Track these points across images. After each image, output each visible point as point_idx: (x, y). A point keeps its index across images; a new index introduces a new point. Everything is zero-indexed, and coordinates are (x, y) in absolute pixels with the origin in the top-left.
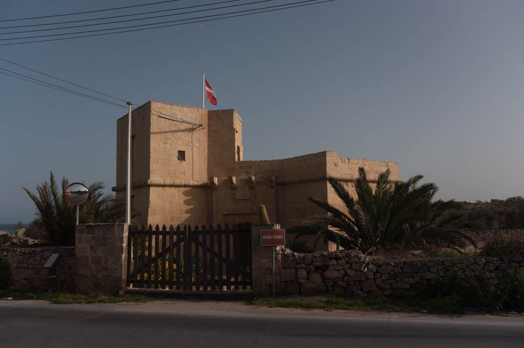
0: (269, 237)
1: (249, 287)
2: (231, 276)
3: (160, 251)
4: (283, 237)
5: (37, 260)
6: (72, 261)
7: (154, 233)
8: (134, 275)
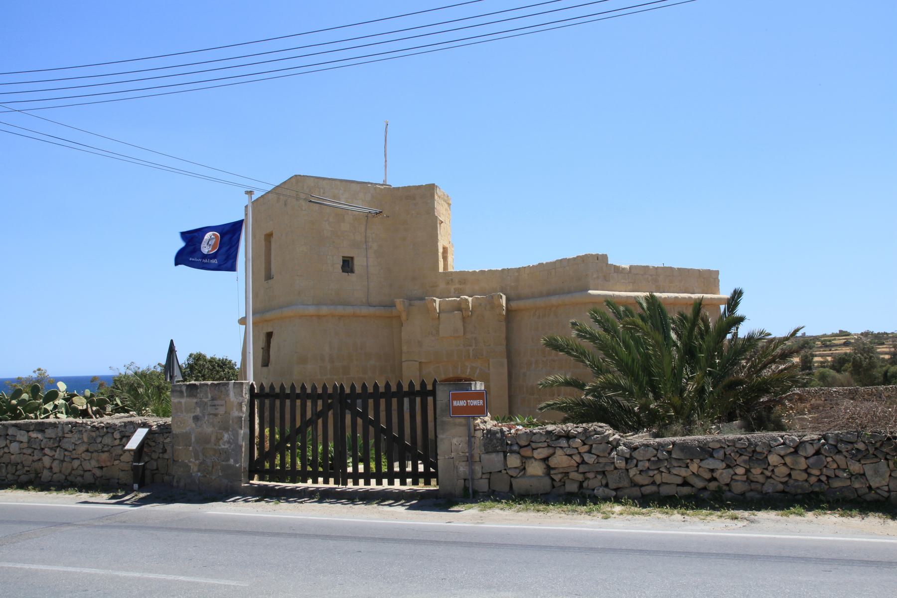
0: (462, 403)
1: (433, 481)
2: (359, 463)
3: (298, 424)
4: (484, 403)
5: (116, 439)
6: (168, 440)
7: (298, 396)
8: (261, 461)
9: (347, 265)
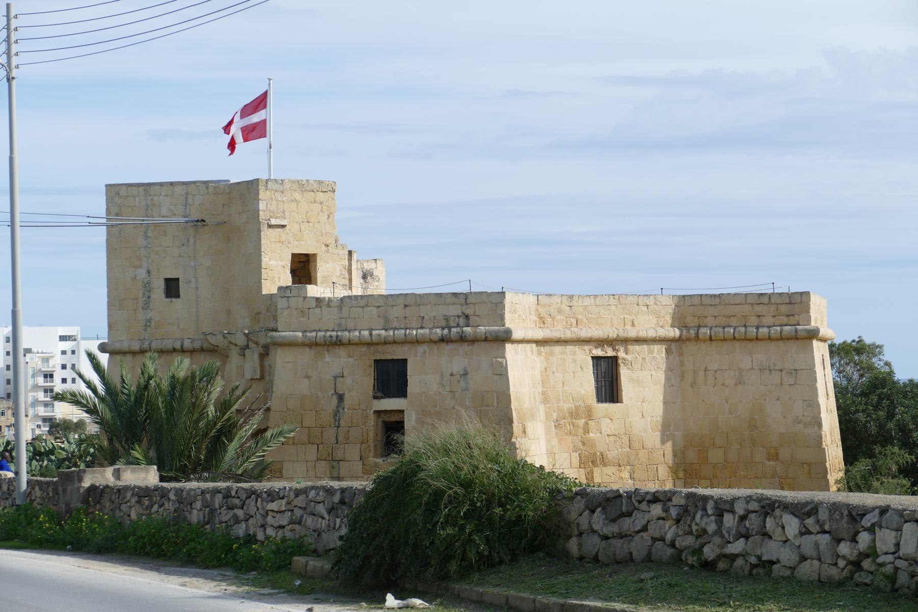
9: (172, 288)
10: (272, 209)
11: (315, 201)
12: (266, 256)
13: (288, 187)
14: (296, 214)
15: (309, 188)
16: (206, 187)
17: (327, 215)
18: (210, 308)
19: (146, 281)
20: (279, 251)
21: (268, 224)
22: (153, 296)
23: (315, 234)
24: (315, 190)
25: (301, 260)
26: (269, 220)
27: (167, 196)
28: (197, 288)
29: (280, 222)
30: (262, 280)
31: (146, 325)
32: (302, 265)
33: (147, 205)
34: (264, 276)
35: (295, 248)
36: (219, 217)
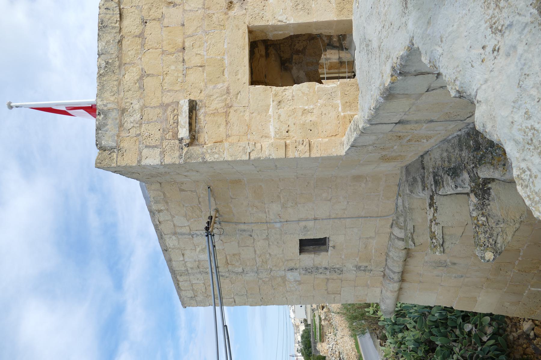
10: (158, 135)
11: (141, 35)
12: (258, 145)
13: (112, 99)
14: (167, 78)
15: (113, 49)
16: (159, 212)
17: (168, 7)
18: (348, 202)
19: (304, 272)
20: (247, 114)
21: (188, 145)
22: (325, 264)
23: (207, 33)
24: (118, 38)
25: (263, 53)
26: (181, 140)
27: (183, 255)
28: (315, 219)
29: (184, 115)
30: (313, 155)
31: (364, 270)
32: (272, 51)
33: (200, 272)
34: (301, 152)
35: (239, 76)
36: (202, 195)
